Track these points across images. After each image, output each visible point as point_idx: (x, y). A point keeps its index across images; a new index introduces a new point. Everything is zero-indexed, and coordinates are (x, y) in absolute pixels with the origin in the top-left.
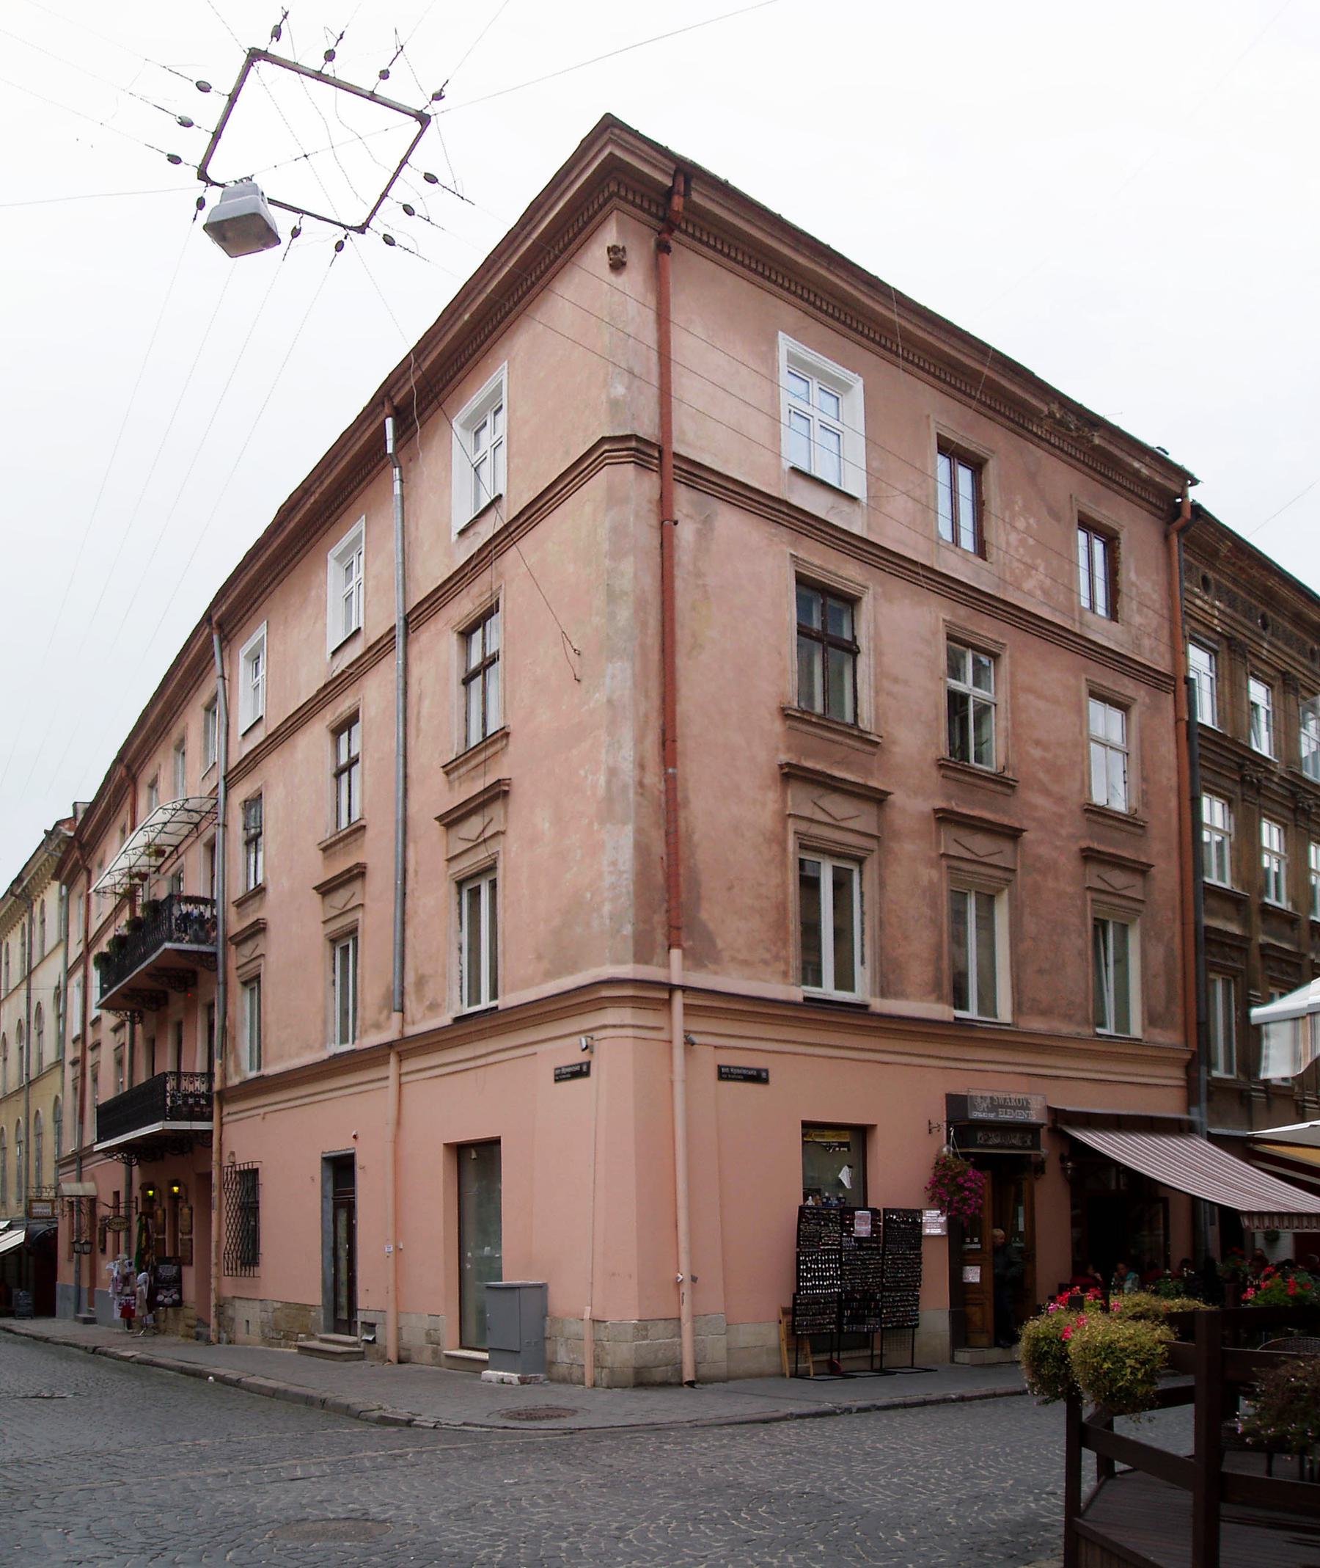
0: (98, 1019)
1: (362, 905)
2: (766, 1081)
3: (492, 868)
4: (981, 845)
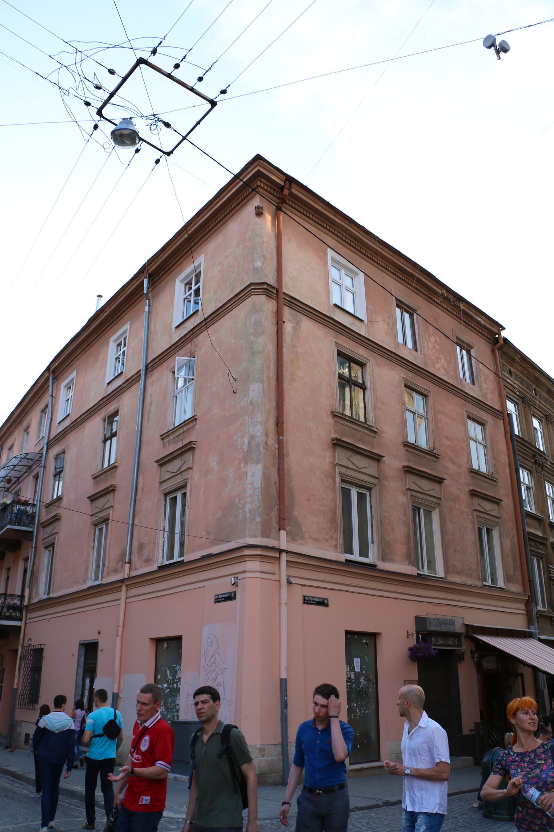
1: (112, 506)
2: (327, 605)
3: (184, 486)
4: (425, 485)
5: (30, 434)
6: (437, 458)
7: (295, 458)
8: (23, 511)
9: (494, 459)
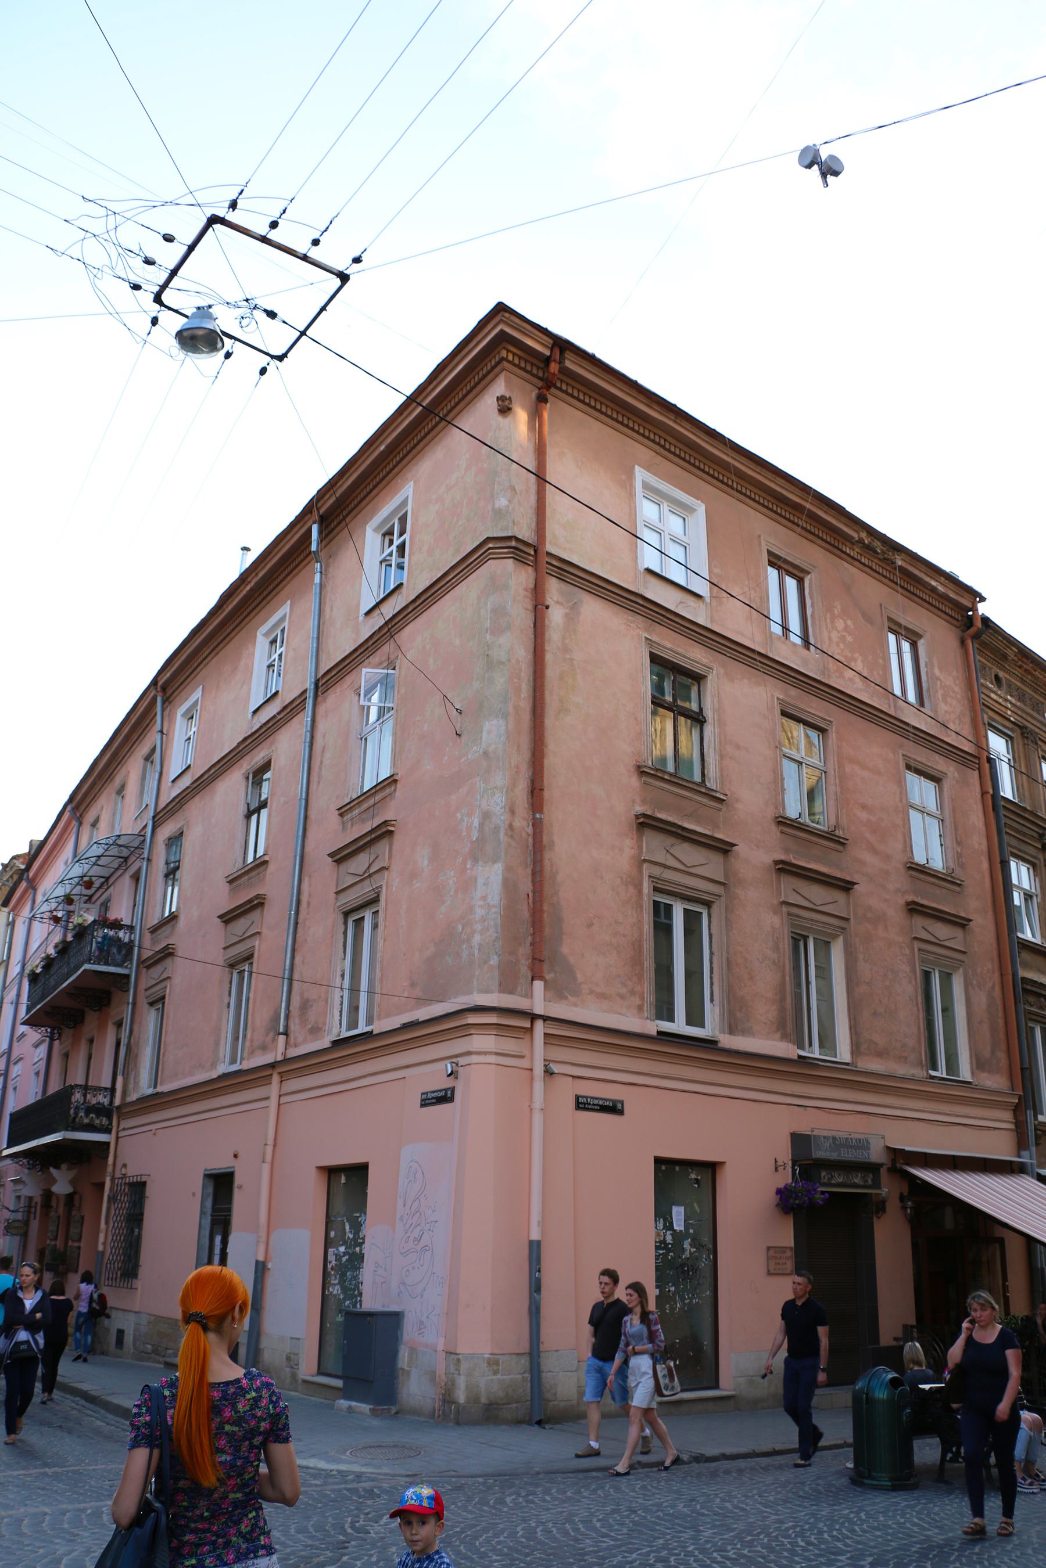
0: (23, 1035)
1: (258, 933)
2: (621, 1112)
3: (375, 900)
4: (817, 894)
5: (128, 798)
6: (843, 844)
7: (565, 850)
8: (111, 939)
9: (958, 843)
